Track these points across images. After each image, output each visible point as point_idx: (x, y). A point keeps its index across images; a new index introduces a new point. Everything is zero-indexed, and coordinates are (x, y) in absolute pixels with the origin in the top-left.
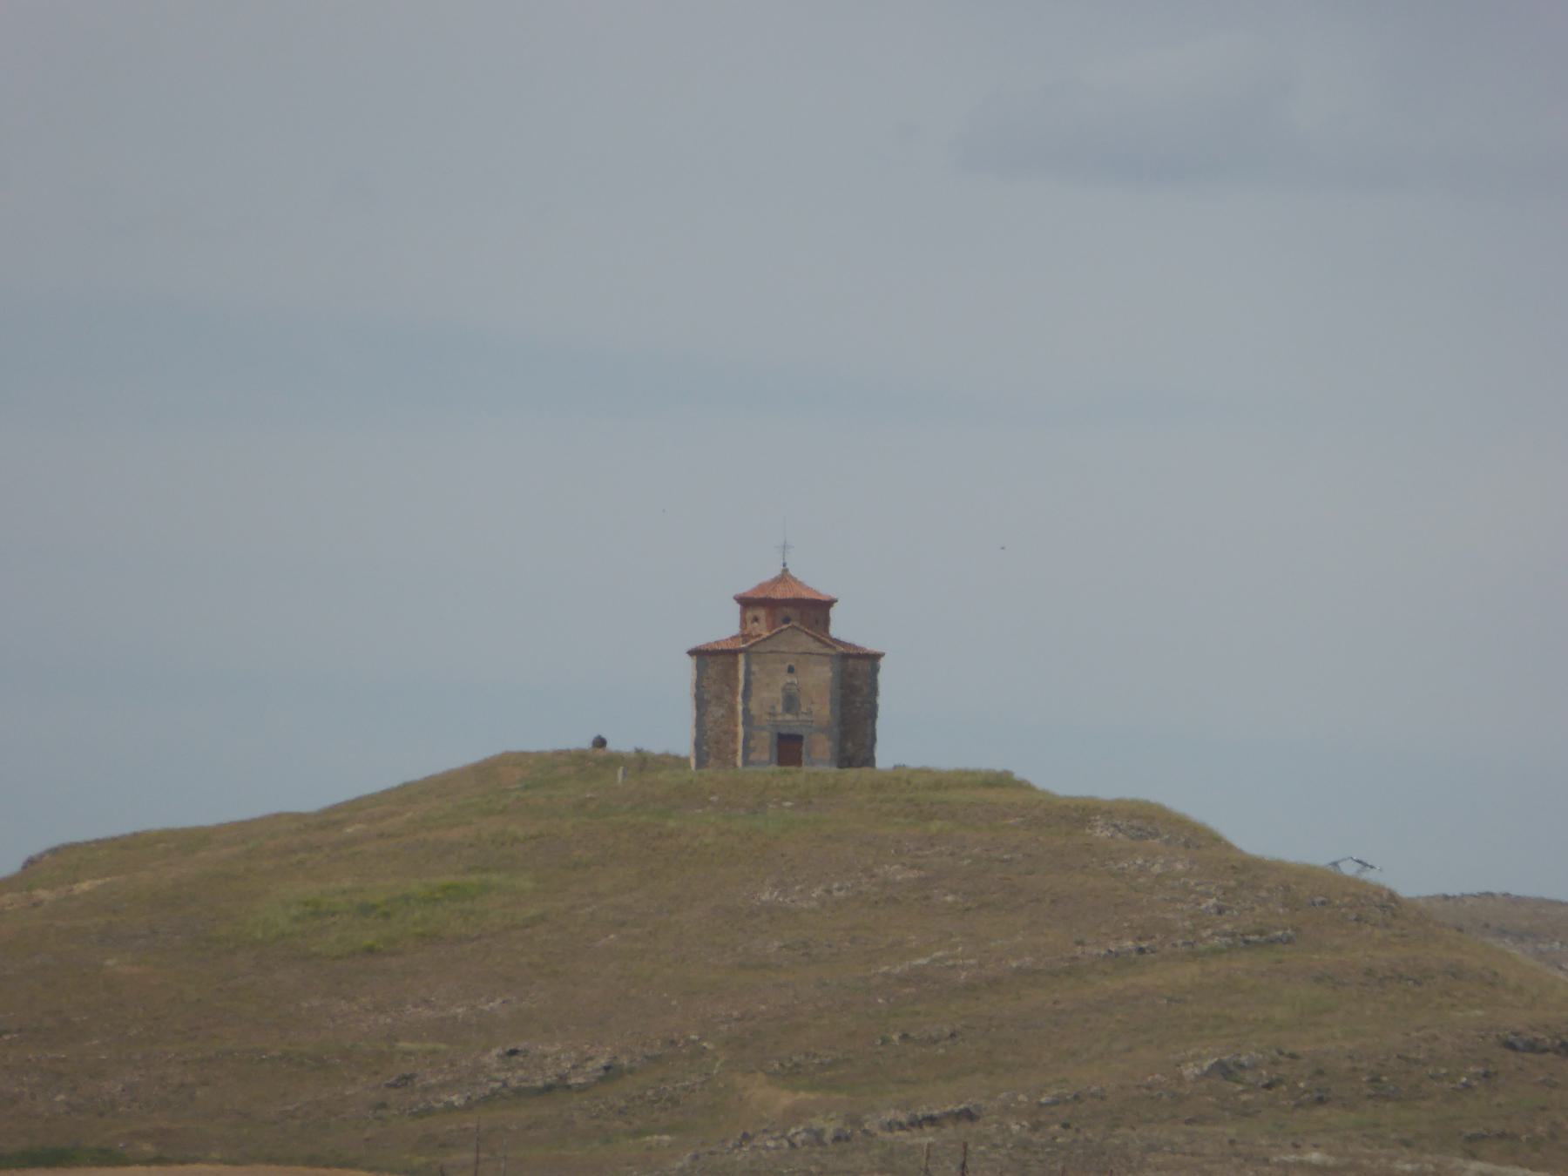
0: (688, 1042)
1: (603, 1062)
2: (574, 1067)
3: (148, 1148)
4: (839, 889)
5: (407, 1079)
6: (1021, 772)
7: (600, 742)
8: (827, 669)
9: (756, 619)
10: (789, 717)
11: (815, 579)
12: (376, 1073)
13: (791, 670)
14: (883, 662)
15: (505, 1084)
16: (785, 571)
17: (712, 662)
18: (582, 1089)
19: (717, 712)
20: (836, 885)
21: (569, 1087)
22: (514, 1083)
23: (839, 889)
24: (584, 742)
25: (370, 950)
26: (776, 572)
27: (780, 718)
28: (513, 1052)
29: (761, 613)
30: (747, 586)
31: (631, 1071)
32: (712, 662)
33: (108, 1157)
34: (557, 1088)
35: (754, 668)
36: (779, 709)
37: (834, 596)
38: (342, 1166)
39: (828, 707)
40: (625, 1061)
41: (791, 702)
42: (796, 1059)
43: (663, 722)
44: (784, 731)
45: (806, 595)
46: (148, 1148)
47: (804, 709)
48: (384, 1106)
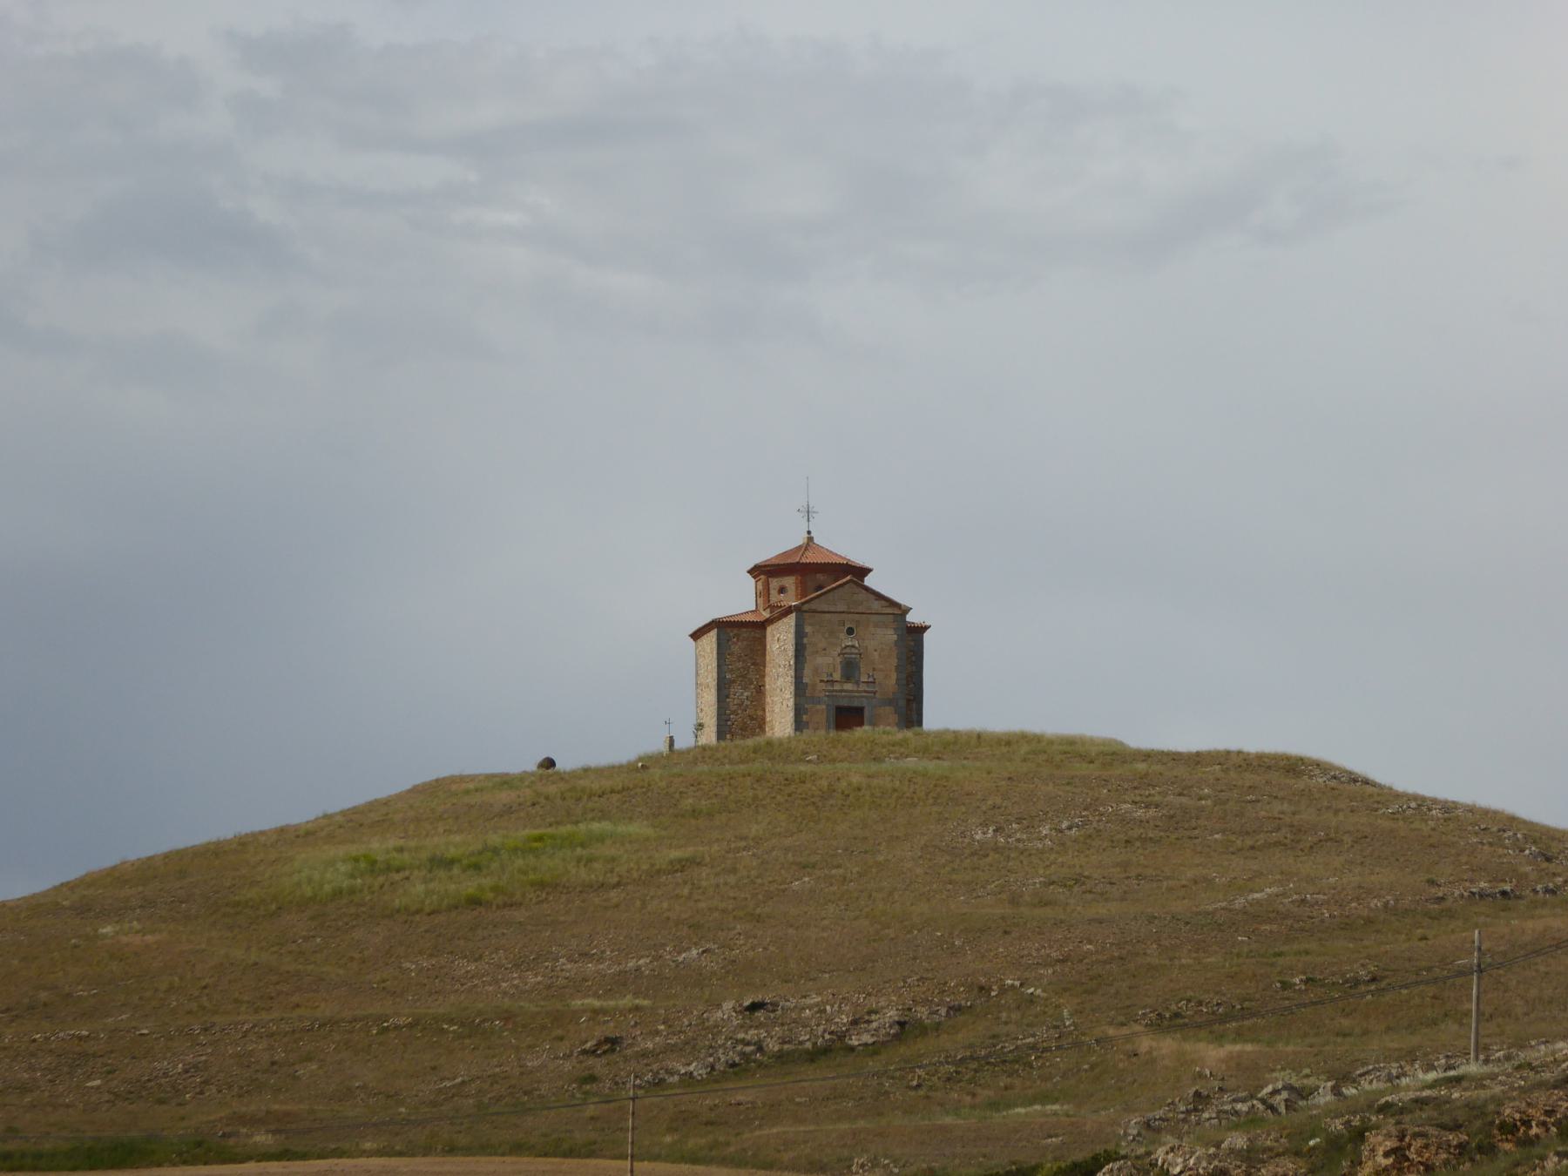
0: (1003, 990)
1: (892, 1014)
2: (855, 1022)
3: (262, 1139)
4: (1070, 828)
5: (613, 1042)
7: (549, 763)
9: (782, 590)
10: (848, 686)
11: (841, 544)
12: (561, 1039)
13: (850, 631)
15: (760, 1049)
16: (810, 539)
17: (736, 642)
18: (873, 1050)
19: (740, 694)
21: (852, 1049)
22: (773, 1046)
23: (1070, 828)
24: (530, 764)
25: (474, 902)
26: (800, 540)
27: (837, 687)
28: (754, 1007)
29: (790, 582)
30: (768, 552)
31: (937, 1027)
33: (201, 1150)
34: (831, 1050)
35: (808, 629)
36: (837, 676)
37: (867, 565)
38: (570, 1153)
39: (894, 676)
40: (922, 1012)
42: (1173, 1007)
43: (667, 706)
44: (844, 703)
46: (262, 1139)
48: (592, 1079)
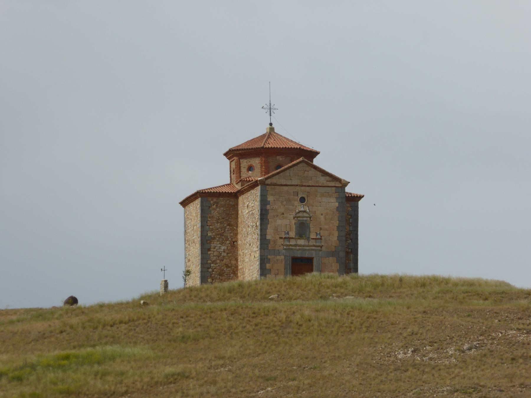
4: (470, 349)
6: (508, 280)
7: (73, 301)
8: (333, 200)
9: (250, 168)
10: (301, 242)
11: (295, 132)
13: (302, 200)
14: (361, 203)
16: (272, 129)
19: (219, 248)
20: (466, 346)
26: (263, 130)
30: (239, 139)
32: (214, 208)
35: (270, 198)
36: (292, 234)
39: (336, 234)
41: (302, 229)
44: (298, 254)
45: (289, 145)
47: (313, 236)
